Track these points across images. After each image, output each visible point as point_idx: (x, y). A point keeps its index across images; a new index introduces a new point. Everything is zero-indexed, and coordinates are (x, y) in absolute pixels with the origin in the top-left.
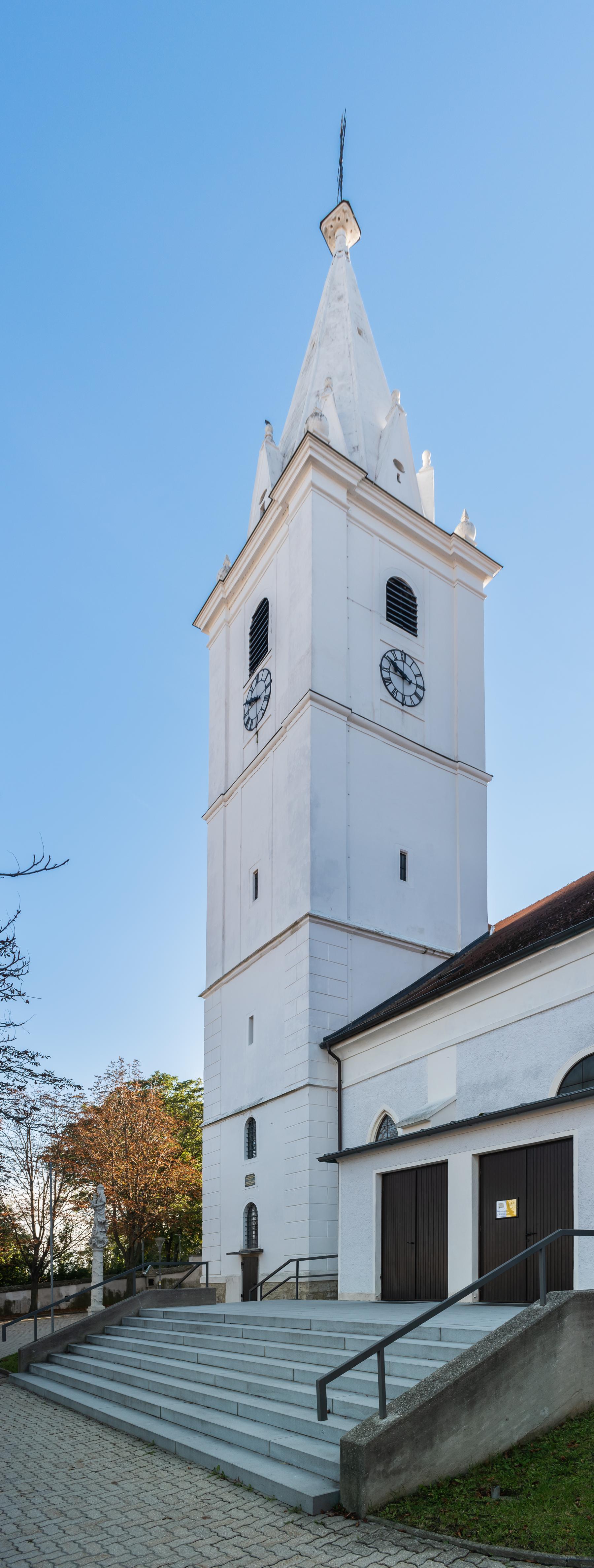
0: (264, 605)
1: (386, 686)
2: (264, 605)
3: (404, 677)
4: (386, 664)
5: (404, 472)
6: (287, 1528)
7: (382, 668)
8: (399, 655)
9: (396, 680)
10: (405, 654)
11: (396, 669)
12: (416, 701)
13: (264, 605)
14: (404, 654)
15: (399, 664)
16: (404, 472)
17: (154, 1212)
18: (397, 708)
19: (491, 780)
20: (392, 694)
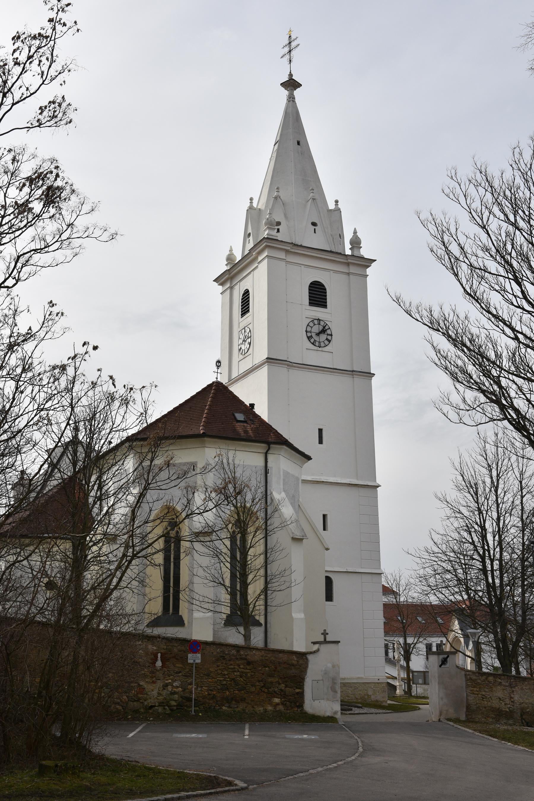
7: (306, 331)
12: (327, 343)
20: (313, 344)
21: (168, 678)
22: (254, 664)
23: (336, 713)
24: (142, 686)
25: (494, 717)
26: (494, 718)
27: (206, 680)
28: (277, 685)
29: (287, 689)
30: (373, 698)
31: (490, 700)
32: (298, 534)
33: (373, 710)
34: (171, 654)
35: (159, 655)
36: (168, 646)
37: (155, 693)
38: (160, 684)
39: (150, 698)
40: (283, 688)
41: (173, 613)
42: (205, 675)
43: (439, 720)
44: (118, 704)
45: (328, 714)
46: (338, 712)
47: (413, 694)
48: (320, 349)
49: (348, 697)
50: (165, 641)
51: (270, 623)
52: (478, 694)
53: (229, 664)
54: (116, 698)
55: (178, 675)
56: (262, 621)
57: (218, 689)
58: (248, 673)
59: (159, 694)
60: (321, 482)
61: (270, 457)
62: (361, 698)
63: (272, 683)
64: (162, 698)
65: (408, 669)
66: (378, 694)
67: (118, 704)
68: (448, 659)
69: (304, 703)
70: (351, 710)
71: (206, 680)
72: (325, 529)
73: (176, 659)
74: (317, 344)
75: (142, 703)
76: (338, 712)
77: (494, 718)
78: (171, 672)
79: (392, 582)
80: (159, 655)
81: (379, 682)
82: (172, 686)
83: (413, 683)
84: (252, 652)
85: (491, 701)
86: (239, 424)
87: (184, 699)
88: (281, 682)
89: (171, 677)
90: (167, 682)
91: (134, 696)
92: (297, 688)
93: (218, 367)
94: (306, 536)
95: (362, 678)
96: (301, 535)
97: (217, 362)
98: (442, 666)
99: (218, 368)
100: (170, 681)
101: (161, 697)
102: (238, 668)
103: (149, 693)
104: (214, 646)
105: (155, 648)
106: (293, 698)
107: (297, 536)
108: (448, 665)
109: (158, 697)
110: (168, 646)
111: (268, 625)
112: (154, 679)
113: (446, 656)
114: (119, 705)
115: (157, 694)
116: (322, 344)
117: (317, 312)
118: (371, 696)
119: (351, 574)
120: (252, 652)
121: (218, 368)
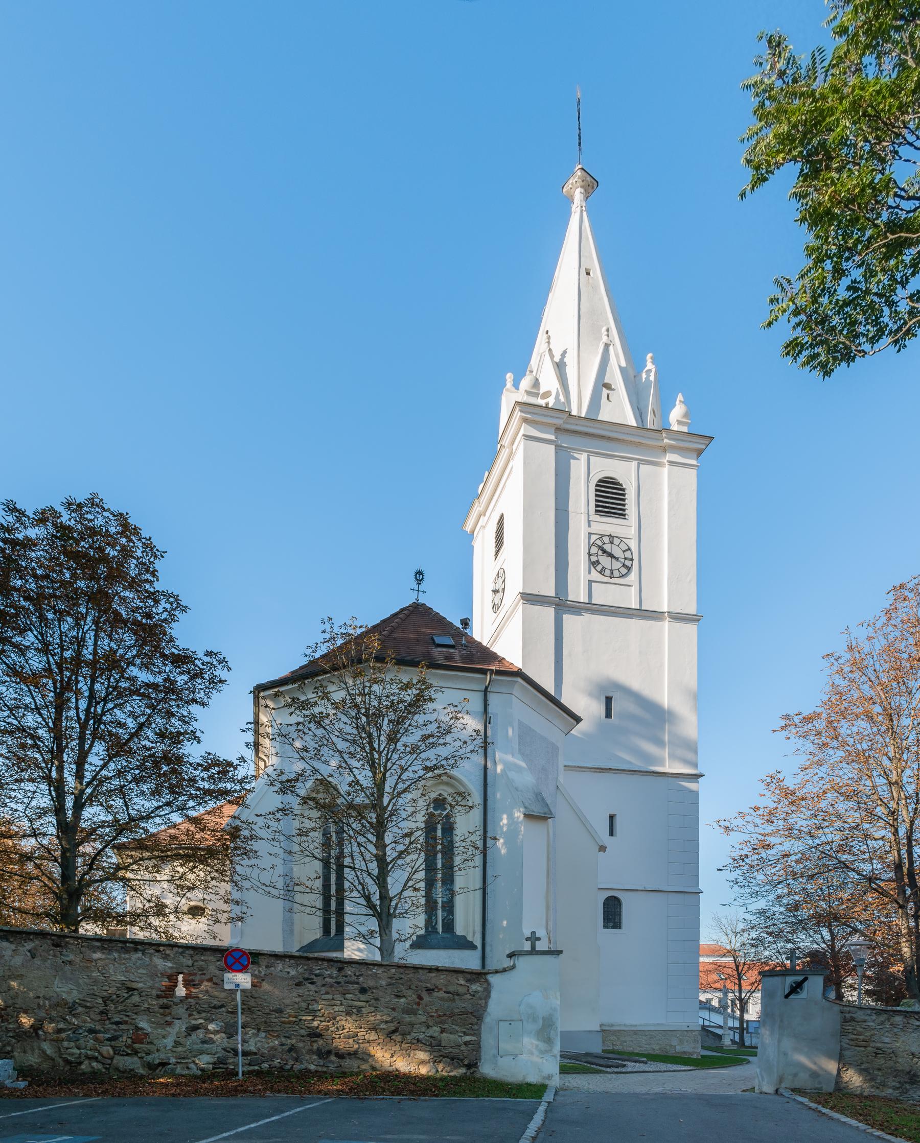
0: (502, 516)
1: (603, 575)
2: (502, 516)
3: (610, 555)
4: (594, 550)
5: (614, 390)
6: (433, 987)
7: (590, 554)
8: (606, 540)
9: (605, 561)
10: (613, 537)
11: (604, 551)
12: (624, 571)
13: (502, 516)
14: (612, 537)
15: (607, 547)
16: (614, 390)
17: (872, 897)
18: (602, 582)
19: (598, 482)
20: (600, 572)
21: (196, 1017)
22: (374, 991)
23: (550, 1077)
24: (142, 1029)
25: (898, 1085)
26: (898, 1088)
27: (276, 1020)
28: (423, 1029)
29: (444, 1035)
30: (679, 1049)
31: (891, 1057)
32: (535, 810)
33: (663, 1066)
34: (202, 974)
35: (180, 977)
36: (197, 961)
37: (169, 1042)
38: (179, 1027)
39: (158, 1050)
40: (436, 1035)
41: (336, 935)
42: (273, 1011)
43: (777, 1091)
44: (96, 1059)
45: (533, 1079)
46: (552, 1076)
47: (746, 1044)
48: (613, 580)
49: (640, 1047)
50: (192, 952)
51: (491, 946)
52: (865, 1047)
53: (322, 993)
54: (91, 1050)
55: (218, 1011)
56: (478, 942)
57: (302, 1036)
58: (362, 1007)
59: (177, 1043)
60: (606, 769)
61: (493, 699)
62: (660, 1049)
63: (412, 1025)
64: (184, 1049)
65: (741, 1019)
66: (686, 1044)
67: (96, 1059)
68: (806, 984)
69: (480, 1059)
70: (624, 1066)
71: (276, 1020)
72: (612, 833)
73: (214, 983)
74: (607, 572)
75: (142, 1058)
76: (552, 1076)
77: (898, 1088)
78: (204, 1006)
79: (727, 926)
80: (180, 977)
81: (688, 1029)
82: (207, 1029)
83: (747, 1033)
84: (371, 970)
85: (894, 1058)
86: (439, 649)
87: (229, 1052)
88: (430, 1024)
89: (204, 1015)
90: (194, 1022)
91: (127, 1047)
92: (465, 1034)
93: (419, 582)
94: (552, 814)
95: (662, 1024)
96: (542, 811)
97: (417, 573)
98: (792, 997)
99: (419, 584)
100: (202, 1021)
101: (180, 1049)
102: (342, 999)
103: (155, 1042)
104: (292, 961)
105: (169, 964)
106: (458, 1051)
107: (533, 811)
108: (803, 995)
109: (174, 1049)
110: (197, 961)
111: (488, 949)
112: (168, 1018)
113: (800, 978)
114: (97, 1062)
115: (172, 1044)
116: (616, 573)
117: (608, 525)
118: (675, 1046)
119: (651, 893)
120: (371, 970)
121: (419, 584)
